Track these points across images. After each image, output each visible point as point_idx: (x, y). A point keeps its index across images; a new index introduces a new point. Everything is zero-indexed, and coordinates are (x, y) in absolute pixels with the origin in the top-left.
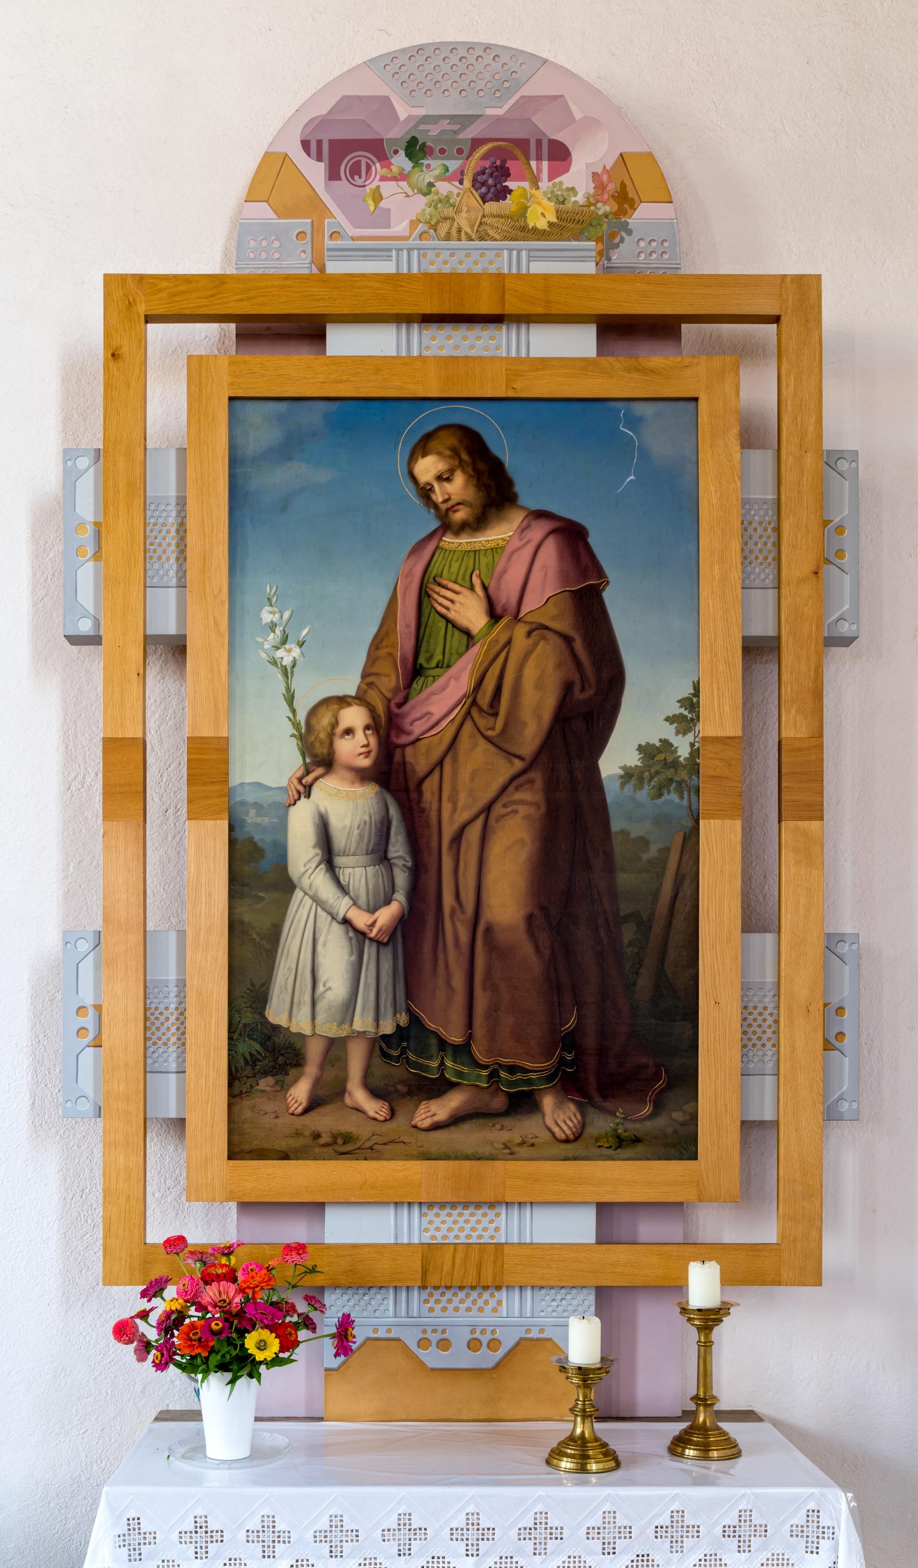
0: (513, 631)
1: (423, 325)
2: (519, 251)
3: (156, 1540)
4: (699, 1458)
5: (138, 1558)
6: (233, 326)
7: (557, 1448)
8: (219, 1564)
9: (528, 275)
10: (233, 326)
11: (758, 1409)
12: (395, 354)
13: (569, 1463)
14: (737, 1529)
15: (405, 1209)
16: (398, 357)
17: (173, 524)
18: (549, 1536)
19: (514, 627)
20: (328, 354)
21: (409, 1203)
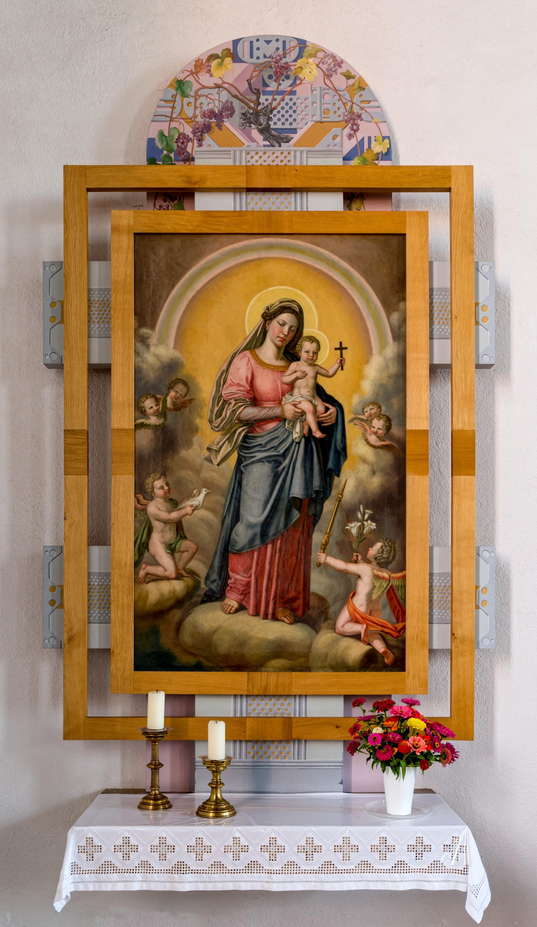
0: (290, 364)
1: (248, 193)
2: (301, 152)
3: (97, 853)
4: (231, 816)
5: (91, 859)
6: (146, 193)
7: (203, 806)
8: (184, 859)
9: (307, 166)
10: (146, 193)
11: (433, 789)
12: (232, 210)
13: (225, 815)
14: (415, 847)
15: (293, 698)
16: (235, 212)
17: (436, 593)
18: (342, 847)
19: (291, 362)
20: (196, 209)
21: (300, 696)
